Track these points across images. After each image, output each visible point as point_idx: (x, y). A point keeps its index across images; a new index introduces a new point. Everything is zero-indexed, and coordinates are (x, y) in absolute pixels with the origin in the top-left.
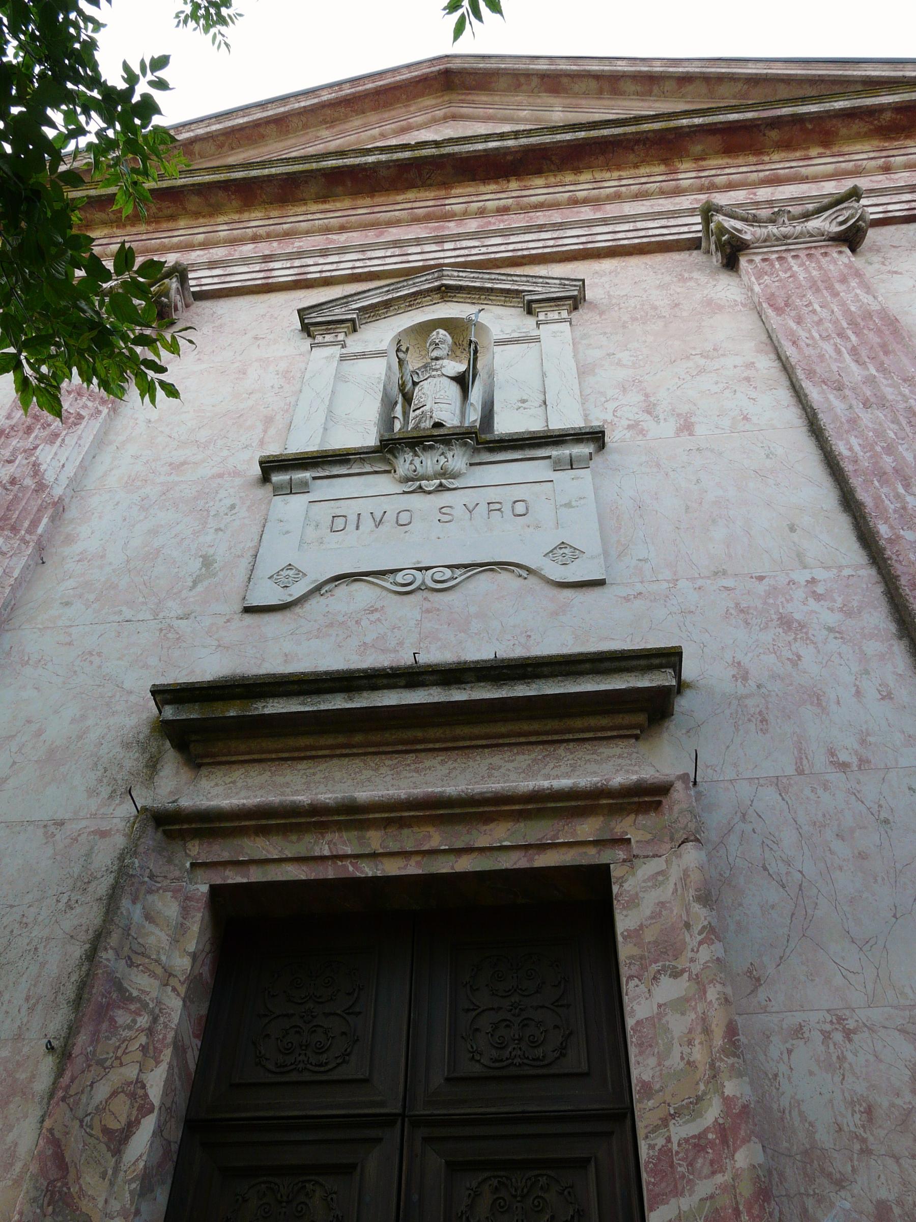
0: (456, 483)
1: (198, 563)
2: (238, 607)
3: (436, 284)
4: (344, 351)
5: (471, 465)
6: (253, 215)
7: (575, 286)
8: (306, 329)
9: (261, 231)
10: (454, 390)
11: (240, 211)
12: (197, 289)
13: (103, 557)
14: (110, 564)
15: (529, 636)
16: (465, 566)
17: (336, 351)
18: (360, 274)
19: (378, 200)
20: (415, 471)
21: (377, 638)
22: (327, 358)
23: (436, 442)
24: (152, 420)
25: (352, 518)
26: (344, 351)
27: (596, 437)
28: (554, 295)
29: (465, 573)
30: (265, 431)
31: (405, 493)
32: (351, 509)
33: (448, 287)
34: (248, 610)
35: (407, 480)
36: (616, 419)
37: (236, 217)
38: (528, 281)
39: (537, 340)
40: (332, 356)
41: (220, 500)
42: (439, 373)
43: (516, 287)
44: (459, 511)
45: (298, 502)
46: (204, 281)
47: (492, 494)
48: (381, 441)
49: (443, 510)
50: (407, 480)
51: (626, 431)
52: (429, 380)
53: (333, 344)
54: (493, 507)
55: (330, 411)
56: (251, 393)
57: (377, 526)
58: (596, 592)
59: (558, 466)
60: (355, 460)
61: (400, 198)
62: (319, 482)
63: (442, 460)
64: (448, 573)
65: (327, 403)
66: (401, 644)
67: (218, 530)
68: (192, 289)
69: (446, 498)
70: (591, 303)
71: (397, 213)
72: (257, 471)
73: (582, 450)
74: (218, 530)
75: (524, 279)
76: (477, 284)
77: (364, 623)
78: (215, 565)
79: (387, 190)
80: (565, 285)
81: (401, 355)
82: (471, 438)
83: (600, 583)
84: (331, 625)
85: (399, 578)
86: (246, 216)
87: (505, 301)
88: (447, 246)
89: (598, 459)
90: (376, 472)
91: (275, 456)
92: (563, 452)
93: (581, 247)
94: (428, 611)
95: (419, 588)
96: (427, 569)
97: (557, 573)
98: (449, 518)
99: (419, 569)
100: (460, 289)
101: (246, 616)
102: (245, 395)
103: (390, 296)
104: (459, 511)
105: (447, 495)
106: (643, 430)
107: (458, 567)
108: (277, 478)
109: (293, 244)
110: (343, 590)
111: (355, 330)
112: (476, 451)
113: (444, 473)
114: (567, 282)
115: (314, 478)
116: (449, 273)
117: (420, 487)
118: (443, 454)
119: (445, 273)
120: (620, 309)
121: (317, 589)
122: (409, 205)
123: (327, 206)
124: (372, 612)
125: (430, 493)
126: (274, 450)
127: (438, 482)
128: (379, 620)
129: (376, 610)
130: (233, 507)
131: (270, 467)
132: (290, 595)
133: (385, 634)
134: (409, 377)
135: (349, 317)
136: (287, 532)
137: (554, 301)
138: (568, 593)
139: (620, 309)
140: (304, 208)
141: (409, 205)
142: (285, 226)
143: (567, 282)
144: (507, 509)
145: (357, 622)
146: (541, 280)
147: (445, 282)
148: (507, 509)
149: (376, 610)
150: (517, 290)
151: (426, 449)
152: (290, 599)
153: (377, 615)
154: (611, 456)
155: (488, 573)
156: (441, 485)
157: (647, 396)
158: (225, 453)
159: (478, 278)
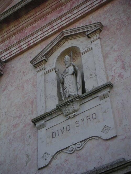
0: (78, 113)
1: (25, 157)
2: (37, 169)
3: (63, 37)
4: (45, 71)
5: (81, 105)
6: (11, 26)
7: (98, 25)
8: (35, 66)
9: (15, 31)
10: (73, 77)
11: (8, 27)
12: (5, 60)
13: (5, 162)
14: (7, 163)
15: (101, 159)
16: (84, 140)
17: (43, 72)
18: (43, 39)
19: (42, 7)
20: (67, 113)
21: (68, 169)
22: (41, 75)
23: (70, 102)
24: (6, 112)
25: (57, 132)
26: (45, 71)
27: (109, 86)
28: (94, 30)
29: (84, 142)
30: (32, 107)
31: (67, 120)
32: (55, 129)
33: (66, 36)
34: (39, 169)
35: (66, 115)
36: (115, 74)
37: (7, 29)
38: (85, 28)
39: (92, 49)
40: (42, 74)
41: (27, 135)
42: (68, 74)
43: (83, 31)
44: (80, 122)
45: (43, 130)
46: (6, 56)
47: (87, 114)
48: (57, 107)
49: (77, 123)
50: (66, 115)
51: (118, 78)
52: (66, 77)
53: (42, 70)
54: (88, 118)
55: (45, 94)
56: (26, 94)
57: (62, 133)
58: (116, 139)
59: (101, 99)
60: (53, 113)
61: (47, 4)
62: (47, 122)
63: (73, 107)
64: (80, 143)
65: (44, 93)
66: (74, 169)
67: (28, 145)
68: (3, 61)
69: (77, 118)
70: (105, 26)
71: (48, 10)
72: (32, 124)
73: (105, 92)
74: (28, 145)
75: (84, 27)
76: (73, 33)
77: (65, 165)
78: (30, 157)
79: (43, 3)
80: (95, 25)
81: (57, 72)
82: (78, 99)
83: (116, 136)
84: (58, 168)
85: (70, 149)
86: (9, 28)
87: (82, 35)
88: (63, 19)
89: (112, 91)
90: (59, 115)
91: (36, 118)
92: (100, 94)
93: (99, 4)
94: (78, 157)
95: (75, 151)
96: (76, 144)
97: (105, 136)
98: (78, 125)
99: (74, 145)
100: (69, 36)
101: (39, 171)
102: (25, 96)
103: (52, 47)
104: (80, 122)
105: (77, 117)
106: (122, 76)
107: (82, 141)
108: (38, 124)
109: (24, 32)
110: (59, 156)
111: (46, 61)
112: (80, 101)
113: (74, 111)
114: (96, 24)
115: (46, 121)
116: (65, 32)
117: (70, 117)
118: (72, 105)
119: (64, 32)
120: (113, 26)
121: (53, 158)
122: (50, 6)
123: (29, 15)
124: (66, 161)
125: (72, 118)
126: (34, 117)
127: (73, 114)
128: (68, 163)
129: (67, 160)
130: (30, 136)
131: (35, 121)
132: (47, 162)
133: (70, 167)
134: (61, 76)
135: (43, 59)
136: (43, 142)
137: (94, 32)
138: (109, 142)
139: (113, 26)
140: (23, 19)
141: (50, 6)
142: (21, 27)
143: (96, 24)
144: (91, 118)
145: (119, 76)
146: (89, 26)
147: (65, 35)
148: (91, 118)
149: (67, 160)
150: (84, 32)
151: (68, 105)
152: (47, 163)
153: (67, 162)
154: (115, 89)
155: (90, 141)
156: (74, 115)
157: (122, 62)
158: (25, 118)
159: (72, 31)
